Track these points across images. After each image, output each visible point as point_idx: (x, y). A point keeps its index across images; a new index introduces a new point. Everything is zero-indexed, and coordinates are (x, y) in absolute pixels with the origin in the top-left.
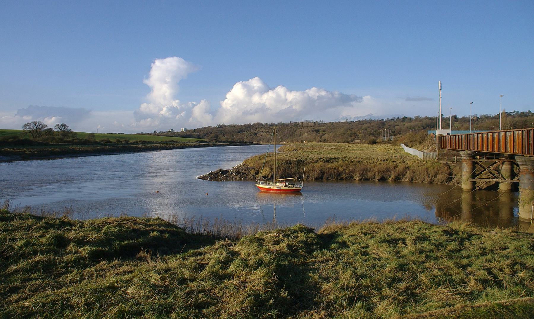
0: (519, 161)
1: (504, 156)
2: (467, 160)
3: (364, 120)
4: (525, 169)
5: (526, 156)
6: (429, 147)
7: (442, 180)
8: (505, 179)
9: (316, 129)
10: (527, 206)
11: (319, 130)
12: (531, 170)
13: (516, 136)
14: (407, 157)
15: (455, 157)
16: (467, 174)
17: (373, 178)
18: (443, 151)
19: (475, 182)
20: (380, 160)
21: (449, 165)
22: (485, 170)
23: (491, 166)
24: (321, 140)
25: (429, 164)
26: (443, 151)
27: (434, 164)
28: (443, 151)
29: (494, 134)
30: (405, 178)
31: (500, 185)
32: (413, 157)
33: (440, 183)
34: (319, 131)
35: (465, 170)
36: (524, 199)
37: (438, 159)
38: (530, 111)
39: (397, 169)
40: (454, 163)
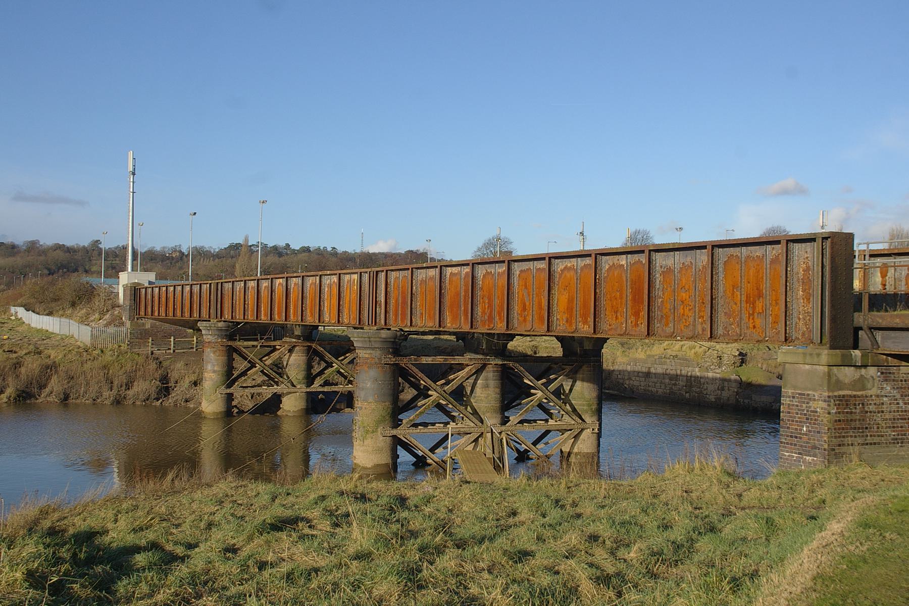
0: (356, 339)
1: (293, 334)
2: (216, 343)
4: (368, 358)
5: (370, 329)
6: (102, 314)
7: (147, 395)
12: (380, 359)
13: (343, 286)
14: (43, 340)
15: (172, 337)
16: (214, 376)
18: (143, 324)
19: (232, 394)
21: (157, 359)
22: (253, 365)
23: (267, 357)
25: (108, 357)
27: (121, 357)
28: (143, 324)
29: (289, 282)
30: (46, 394)
31: (284, 400)
32: (62, 339)
33: (142, 401)
35: (209, 367)
36: (366, 425)
37: (131, 344)
38: (288, 245)
39: (23, 370)
40: (170, 354)
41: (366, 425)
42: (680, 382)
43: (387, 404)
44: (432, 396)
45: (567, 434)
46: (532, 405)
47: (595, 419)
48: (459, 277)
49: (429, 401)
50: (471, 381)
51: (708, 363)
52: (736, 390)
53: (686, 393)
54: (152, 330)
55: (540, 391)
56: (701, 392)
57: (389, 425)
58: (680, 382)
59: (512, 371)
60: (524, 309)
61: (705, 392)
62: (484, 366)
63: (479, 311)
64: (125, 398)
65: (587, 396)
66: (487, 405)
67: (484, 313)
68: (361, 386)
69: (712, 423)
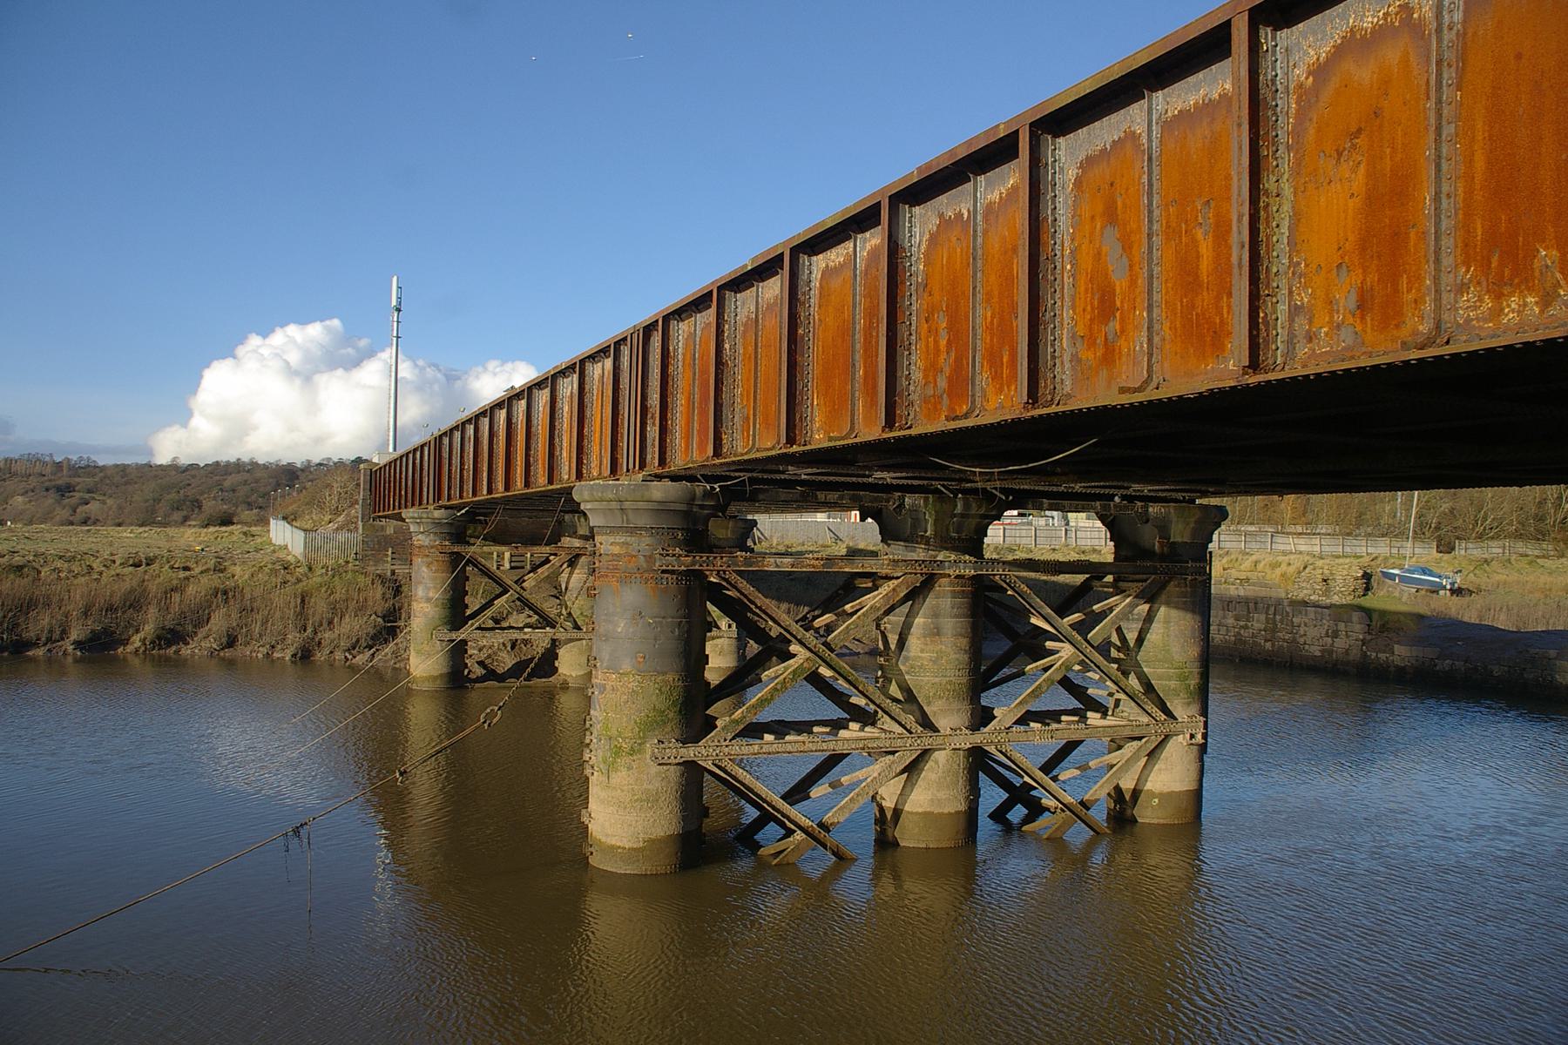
2: (432, 547)
3: (232, 461)
8: (579, 629)
9: (60, 482)
10: (624, 772)
11: (69, 488)
17: (56, 635)
18: (383, 528)
20: (118, 563)
24: (71, 518)
26: (382, 526)
28: (383, 528)
34: (70, 492)
35: (420, 592)
36: (614, 732)
41: (614, 732)
42: (1254, 623)
43: (670, 677)
44: (794, 656)
45: (1130, 748)
46: (1048, 679)
47: (1194, 709)
48: (848, 273)
49: (786, 669)
50: (897, 618)
51: (1305, 591)
52: (1361, 637)
53: (1266, 641)
54: (397, 538)
55: (1067, 646)
56: (1294, 640)
57: (677, 733)
58: (1254, 623)
59: (995, 596)
60: (1105, 306)
61: (1302, 640)
62: (929, 582)
63: (915, 367)
64: (320, 643)
65: (1177, 657)
66: (937, 680)
67: (932, 369)
68: (601, 630)
69: (1308, 699)
